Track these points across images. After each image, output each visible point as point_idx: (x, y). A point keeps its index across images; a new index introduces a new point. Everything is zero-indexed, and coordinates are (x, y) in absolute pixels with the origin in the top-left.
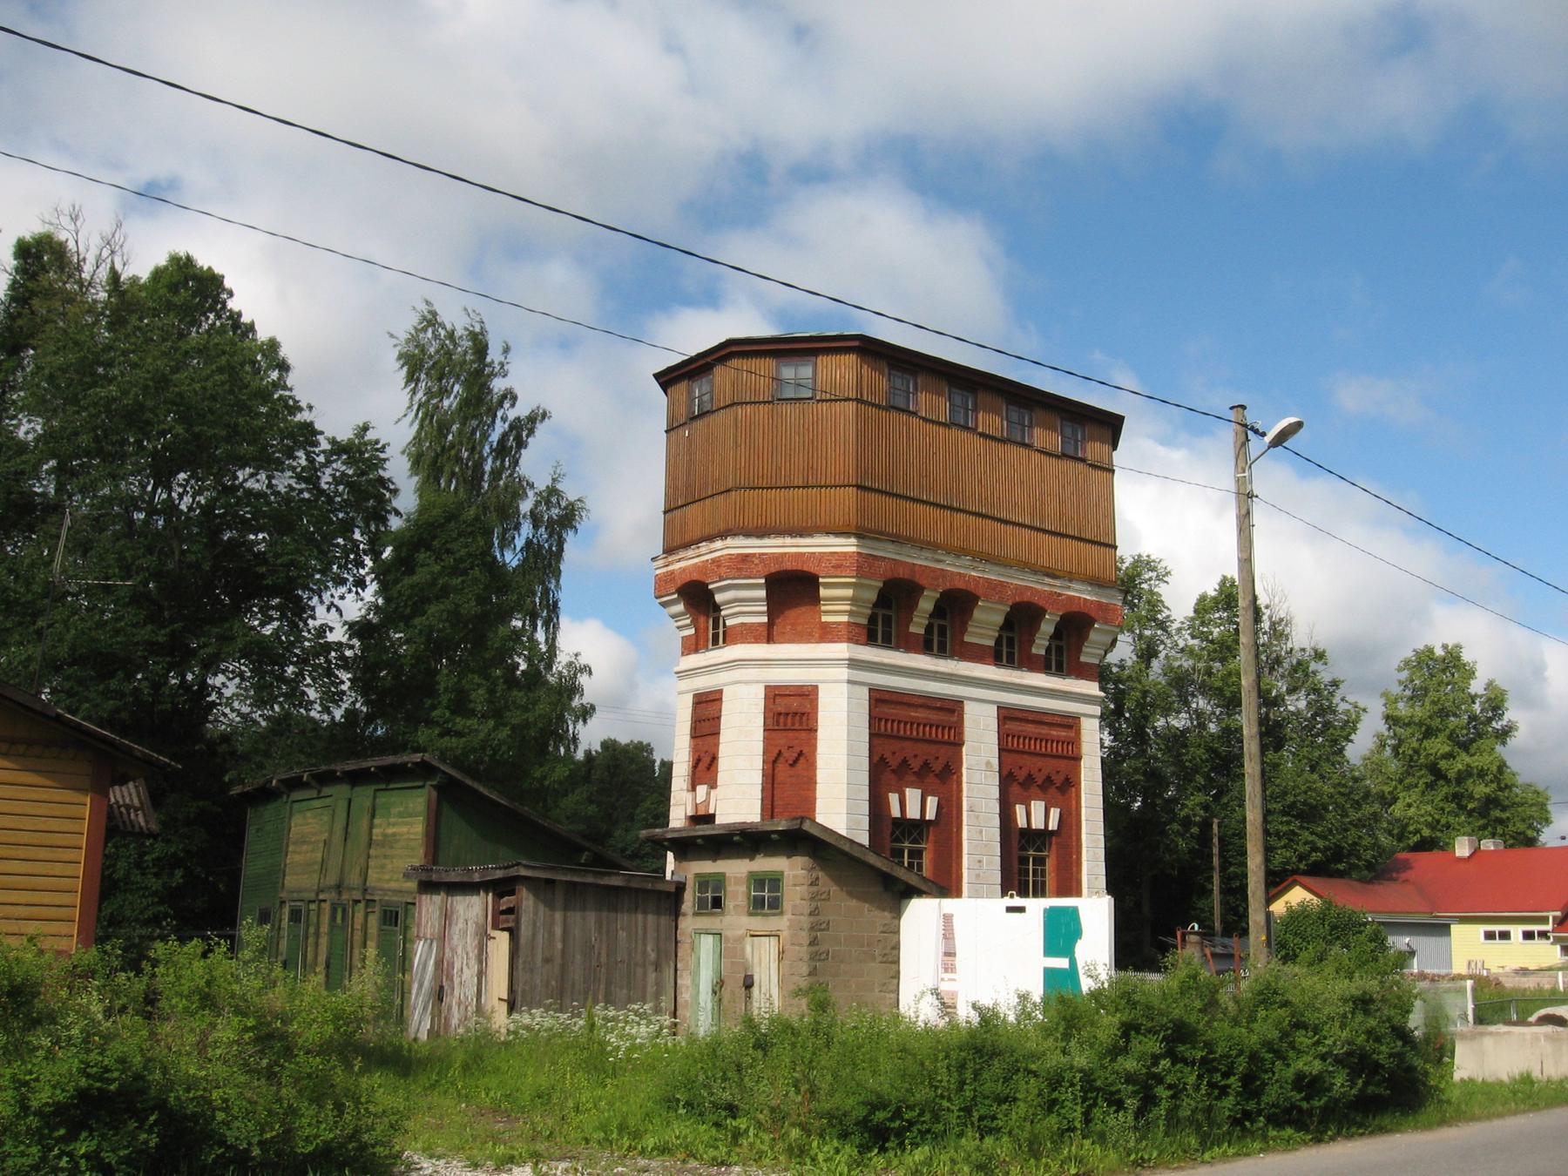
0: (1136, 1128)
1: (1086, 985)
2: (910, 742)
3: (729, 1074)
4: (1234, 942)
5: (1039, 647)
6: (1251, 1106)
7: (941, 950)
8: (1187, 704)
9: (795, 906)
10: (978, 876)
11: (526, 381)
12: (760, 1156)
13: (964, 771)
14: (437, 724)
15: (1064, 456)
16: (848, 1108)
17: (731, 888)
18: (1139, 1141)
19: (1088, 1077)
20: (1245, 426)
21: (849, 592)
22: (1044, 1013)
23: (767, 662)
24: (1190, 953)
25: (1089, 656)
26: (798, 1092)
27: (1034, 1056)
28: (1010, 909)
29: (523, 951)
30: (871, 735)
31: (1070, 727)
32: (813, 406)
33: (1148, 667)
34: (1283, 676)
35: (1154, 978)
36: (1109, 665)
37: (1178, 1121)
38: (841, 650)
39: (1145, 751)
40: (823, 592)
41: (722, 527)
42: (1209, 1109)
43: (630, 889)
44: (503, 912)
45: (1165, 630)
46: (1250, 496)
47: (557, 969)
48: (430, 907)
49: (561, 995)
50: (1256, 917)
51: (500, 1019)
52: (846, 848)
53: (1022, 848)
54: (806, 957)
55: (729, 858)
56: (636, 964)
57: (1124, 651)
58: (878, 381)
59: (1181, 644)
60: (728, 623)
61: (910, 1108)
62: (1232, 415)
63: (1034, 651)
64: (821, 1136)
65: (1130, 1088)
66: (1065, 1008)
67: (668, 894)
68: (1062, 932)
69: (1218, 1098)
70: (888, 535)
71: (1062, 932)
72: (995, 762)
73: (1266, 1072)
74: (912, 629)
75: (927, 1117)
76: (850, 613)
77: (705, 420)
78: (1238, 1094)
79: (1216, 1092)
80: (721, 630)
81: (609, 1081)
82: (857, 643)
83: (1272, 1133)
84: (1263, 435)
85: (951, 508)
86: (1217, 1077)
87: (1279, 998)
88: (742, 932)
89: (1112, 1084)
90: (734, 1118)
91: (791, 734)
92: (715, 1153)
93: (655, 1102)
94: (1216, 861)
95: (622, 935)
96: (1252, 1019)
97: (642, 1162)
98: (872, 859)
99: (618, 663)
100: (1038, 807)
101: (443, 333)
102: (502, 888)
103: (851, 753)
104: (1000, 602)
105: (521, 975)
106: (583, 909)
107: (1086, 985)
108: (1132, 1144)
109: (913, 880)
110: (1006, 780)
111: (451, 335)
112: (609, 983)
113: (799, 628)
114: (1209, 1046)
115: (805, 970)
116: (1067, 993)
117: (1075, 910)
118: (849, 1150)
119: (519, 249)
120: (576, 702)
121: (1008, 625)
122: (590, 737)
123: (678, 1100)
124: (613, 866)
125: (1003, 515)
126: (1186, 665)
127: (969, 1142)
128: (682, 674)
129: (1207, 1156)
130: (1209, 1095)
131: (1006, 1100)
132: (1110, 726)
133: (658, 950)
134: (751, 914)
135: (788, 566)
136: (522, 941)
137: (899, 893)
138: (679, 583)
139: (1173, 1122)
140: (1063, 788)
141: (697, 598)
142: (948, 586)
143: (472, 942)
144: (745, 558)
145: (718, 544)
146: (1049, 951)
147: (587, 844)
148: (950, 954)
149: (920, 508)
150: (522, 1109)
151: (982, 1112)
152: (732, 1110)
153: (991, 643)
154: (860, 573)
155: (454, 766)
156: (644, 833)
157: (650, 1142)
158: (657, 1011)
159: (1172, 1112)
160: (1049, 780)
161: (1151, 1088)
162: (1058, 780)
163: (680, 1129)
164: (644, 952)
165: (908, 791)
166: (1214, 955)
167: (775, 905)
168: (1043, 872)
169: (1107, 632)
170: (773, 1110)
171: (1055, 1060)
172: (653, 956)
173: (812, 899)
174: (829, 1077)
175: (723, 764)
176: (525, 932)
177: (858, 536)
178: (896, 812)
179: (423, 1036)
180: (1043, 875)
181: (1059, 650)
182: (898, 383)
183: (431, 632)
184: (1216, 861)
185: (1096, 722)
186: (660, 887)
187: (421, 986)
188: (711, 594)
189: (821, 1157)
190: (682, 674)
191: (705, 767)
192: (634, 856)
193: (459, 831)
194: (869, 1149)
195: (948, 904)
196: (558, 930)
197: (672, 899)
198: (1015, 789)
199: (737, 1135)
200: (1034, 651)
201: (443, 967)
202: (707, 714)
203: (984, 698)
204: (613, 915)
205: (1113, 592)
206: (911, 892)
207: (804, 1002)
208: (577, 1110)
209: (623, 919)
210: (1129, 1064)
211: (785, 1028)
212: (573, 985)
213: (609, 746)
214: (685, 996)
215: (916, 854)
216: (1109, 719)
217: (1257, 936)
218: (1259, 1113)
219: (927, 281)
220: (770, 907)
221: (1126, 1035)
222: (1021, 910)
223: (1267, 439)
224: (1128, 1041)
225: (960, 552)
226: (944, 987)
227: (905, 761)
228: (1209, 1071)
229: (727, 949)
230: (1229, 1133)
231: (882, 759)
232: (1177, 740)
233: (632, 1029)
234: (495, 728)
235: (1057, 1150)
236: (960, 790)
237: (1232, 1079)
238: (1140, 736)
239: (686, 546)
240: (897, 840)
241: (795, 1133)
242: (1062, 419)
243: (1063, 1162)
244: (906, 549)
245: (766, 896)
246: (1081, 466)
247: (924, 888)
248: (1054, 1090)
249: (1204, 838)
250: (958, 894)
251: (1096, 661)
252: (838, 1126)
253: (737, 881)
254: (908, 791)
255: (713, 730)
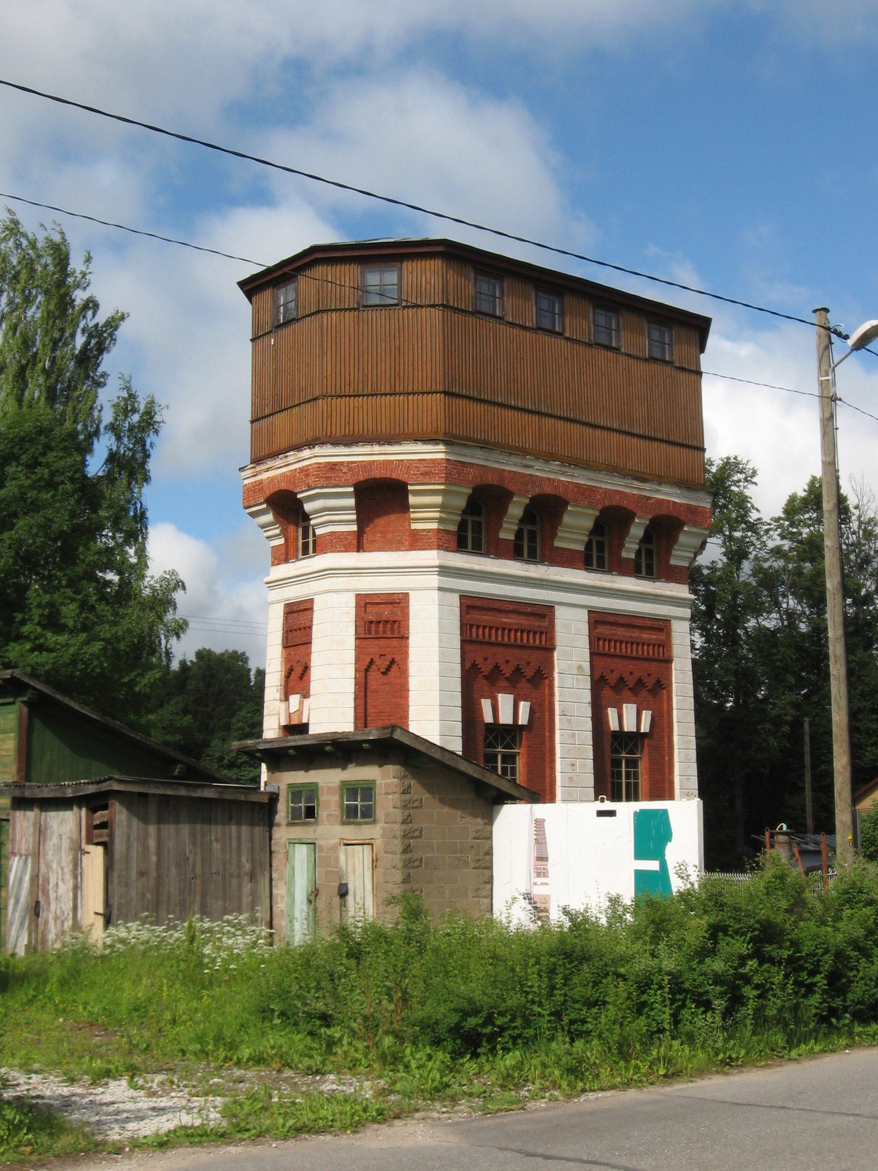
0: (724, 1028)
1: (677, 885)
2: (501, 647)
3: (323, 984)
4: (822, 838)
5: (629, 551)
6: (838, 1003)
7: (534, 855)
8: (778, 604)
9: (387, 815)
10: (571, 779)
11: (110, 287)
12: (355, 1063)
13: (556, 676)
14: (27, 638)
15: (652, 359)
16: (439, 1016)
17: (323, 798)
18: (726, 1040)
19: (676, 979)
20: (828, 329)
21: (438, 499)
22: (635, 914)
23: (357, 571)
24: (779, 853)
25: (679, 559)
26: (391, 1000)
27: (624, 960)
28: (601, 814)
29: (117, 866)
30: (463, 642)
31: (660, 630)
32: (399, 313)
33: (739, 568)
34: (871, 575)
35: (743, 879)
36: (699, 568)
37: (766, 1021)
38: (432, 557)
39: (735, 652)
40: (412, 500)
41: (310, 435)
42: (796, 1008)
43: (223, 801)
44: (97, 827)
45: (755, 532)
46: (834, 399)
47: (152, 883)
48: (24, 822)
49: (156, 908)
50: (842, 816)
51: (98, 935)
52: (438, 756)
53: (615, 751)
54: (400, 865)
55: (321, 768)
56: (231, 875)
57: (714, 553)
58: (466, 286)
59: (771, 544)
60: (319, 532)
61: (502, 1014)
62: (814, 318)
63: (624, 554)
64: (414, 1043)
65: (718, 988)
66: (655, 910)
67: (261, 805)
68: (651, 836)
69: (805, 996)
70: (477, 441)
71: (651, 836)
72: (587, 666)
73: (851, 969)
74: (503, 535)
75: (519, 1022)
76: (440, 520)
77: (296, 326)
78: (824, 992)
79: (803, 990)
80: (311, 539)
81: (205, 992)
82: (447, 550)
83: (858, 1029)
84: (846, 337)
85: (539, 413)
86: (804, 975)
87: (864, 897)
88: (334, 841)
89: (700, 986)
90: (328, 1026)
91: (382, 642)
92: (311, 1062)
93: (251, 1013)
94: (807, 759)
95: (217, 846)
96: (837, 918)
97: (238, 1073)
98: (465, 767)
99: (208, 571)
100: (629, 710)
101: (25, 243)
102: (95, 802)
103: (443, 660)
104: (590, 506)
105: (116, 888)
106: (177, 822)
107: (677, 885)
108: (719, 1044)
109: (505, 786)
110: (598, 684)
111: (33, 245)
112: (204, 895)
113: (389, 536)
114: (795, 945)
115: (398, 876)
116: (656, 897)
117: (665, 813)
118: (441, 1056)
119: (65, 152)
120: (169, 617)
121: (598, 529)
122: (182, 650)
123: (273, 1011)
124: (208, 778)
125: (591, 420)
126: (775, 565)
127: (560, 1046)
128: (274, 584)
129: (794, 1053)
130: (796, 993)
131: (595, 1003)
132: (702, 628)
133: (253, 861)
134: (343, 823)
135: (377, 474)
136: (117, 855)
137: (492, 799)
138: (268, 493)
139: (761, 1021)
140: (653, 691)
141: (287, 507)
142: (537, 491)
143: (66, 858)
144: (333, 467)
145: (306, 453)
146: (640, 853)
147: (178, 756)
148: (542, 858)
149: (509, 414)
150: (119, 1023)
151: (572, 1016)
152: (326, 1019)
153: (581, 548)
154: (449, 479)
155: (48, 682)
156: (236, 744)
157: (246, 1052)
158: (253, 921)
159: (759, 1011)
160: (640, 681)
161: (739, 988)
162: (650, 682)
163: (275, 1039)
164: (239, 864)
165: (501, 697)
166: (803, 852)
167: (368, 814)
168: (636, 773)
169: (697, 535)
170: (366, 1018)
171: (644, 963)
172: (247, 866)
173: (405, 807)
174: (421, 985)
175: (316, 673)
176: (119, 846)
177: (446, 443)
178: (488, 718)
179: (21, 952)
180: (636, 778)
181: (649, 553)
182: (484, 287)
183: (21, 546)
184: (807, 759)
185: (686, 625)
186: (253, 798)
187: (17, 902)
188: (300, 503)
189: (413, 1064)
190: (274, 584)
191: (297, 677)
192: (231, 765)
193: (50, 744)
194: (462, 1055)
195: (540, 810)
196: (152, 844)
197: (264, 811)
198: (607, 693)
199: (331, 1043)
200: (624, 554)
201: (38, 883)
202: (298, 622)
203: (573, 600)
204: (206, 826)
205: (701, 495)
206: (503, 798)
207: (398, 909)
208: (174, 1022)
209: (217, 830)
210: (717, 965)
211: (378, 936)
212: (169, 898)
213: (203, 656)
214: (280, 906)
215: (509, 759)
216: (701, 619)
217: (843, 835)
218: (845, 1009)
219: (481, 176)
220: (364, 816)
221: (714, 937)
222: (611, 813)
223: (850, 342)
224: (716, 943)
225: (548, 457)
226: (537, 891)
227: (497, 667)
228: (795, 970)
229: (321, 858)
230: (816, 1030)
231: (474, 665)
232: (765, 637)
233: (231, 940)
234: (87, 642)
235: (646, 1052)
236: (552, 695)
237: (818, 978)
238: (732, 639)
239: (274, 455)
240: (490, 745)
241: (388, 1041)
242: (649, 322)
243: (652, 1063)
244: (494, 455)
245: (359, 806)
246: (668, 369)
247: (515, 793)
248: (643, 992)
249: (796, 737)
250: (552, 800)
251: (686, 564)
252: (431, 1034)
253: (330, 790)
254: (501, 697)
255: (304, 640)
